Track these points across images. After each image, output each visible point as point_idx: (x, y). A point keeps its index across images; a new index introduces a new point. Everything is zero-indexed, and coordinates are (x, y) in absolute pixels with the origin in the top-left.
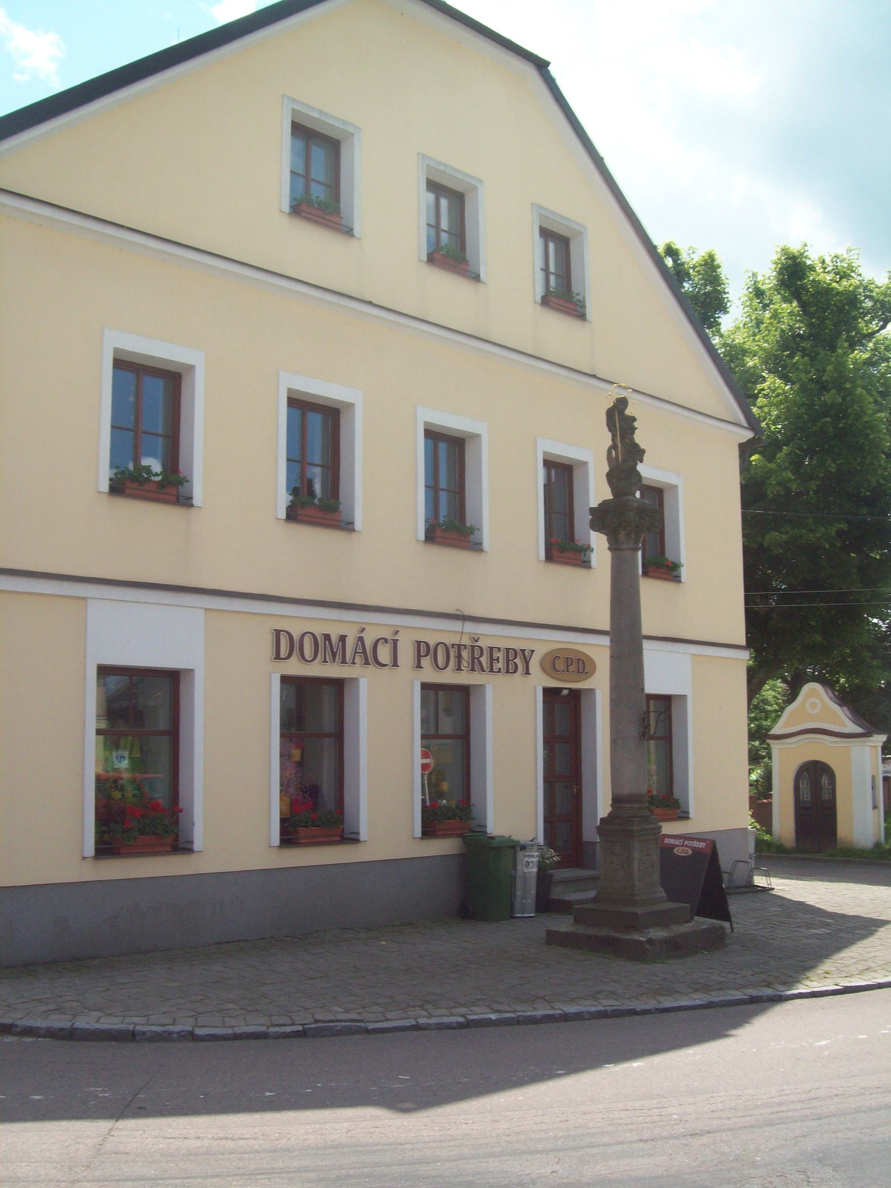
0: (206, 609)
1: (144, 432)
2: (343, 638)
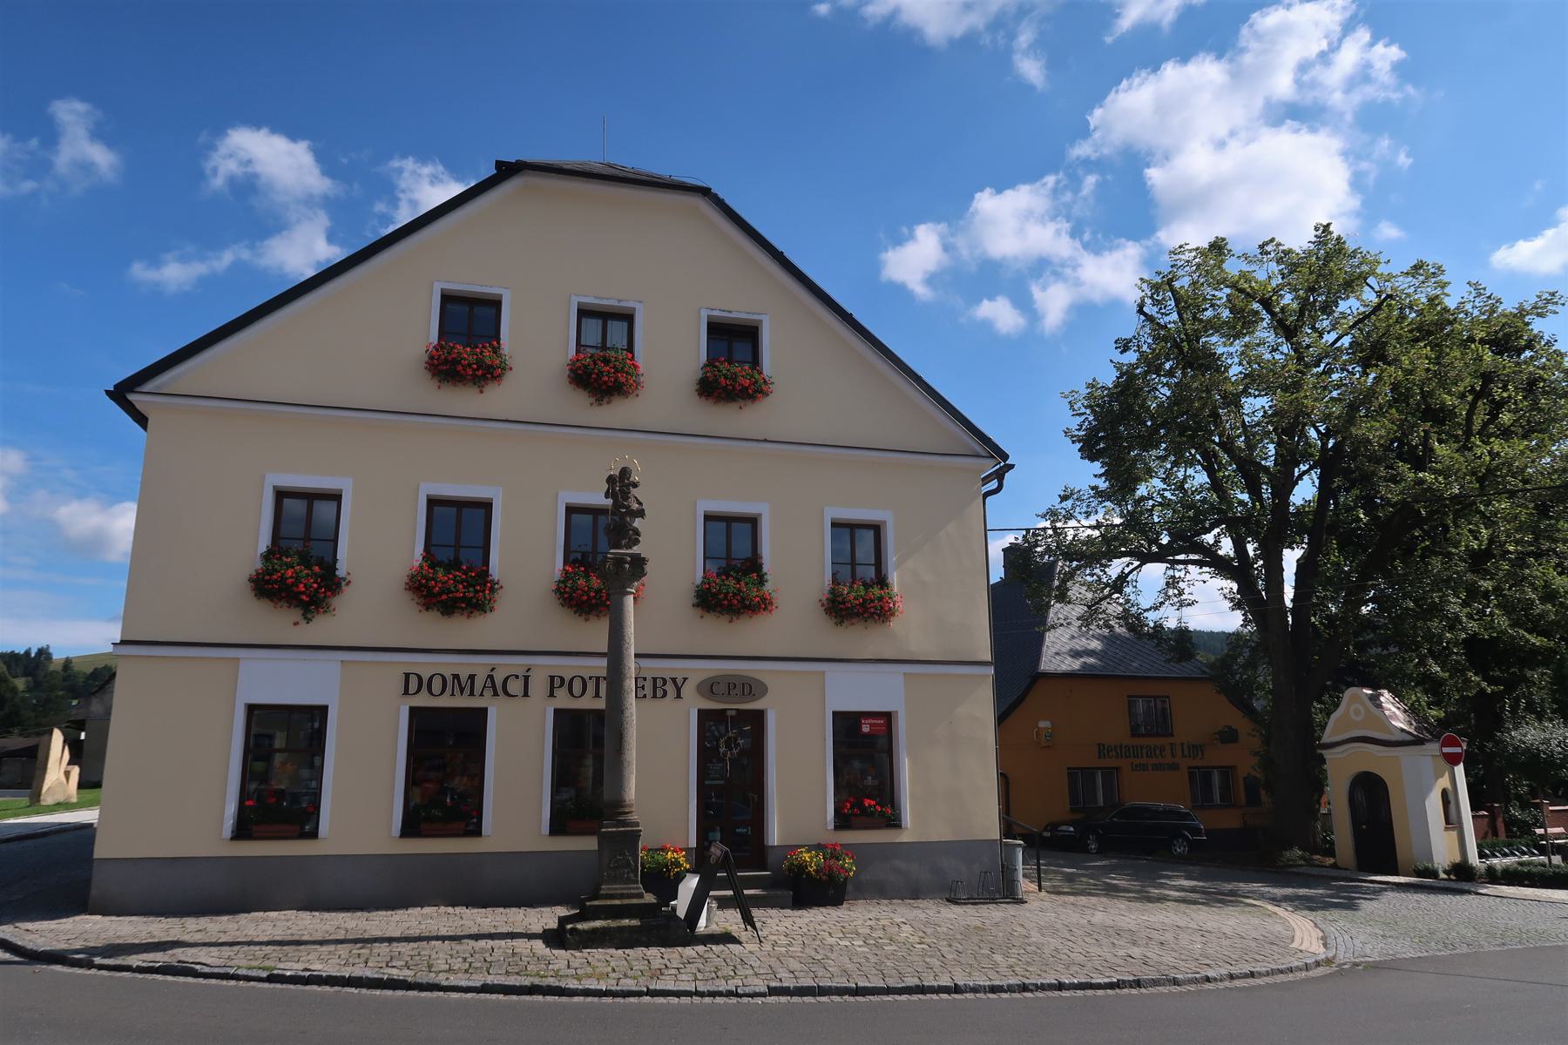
2: (472, 677)
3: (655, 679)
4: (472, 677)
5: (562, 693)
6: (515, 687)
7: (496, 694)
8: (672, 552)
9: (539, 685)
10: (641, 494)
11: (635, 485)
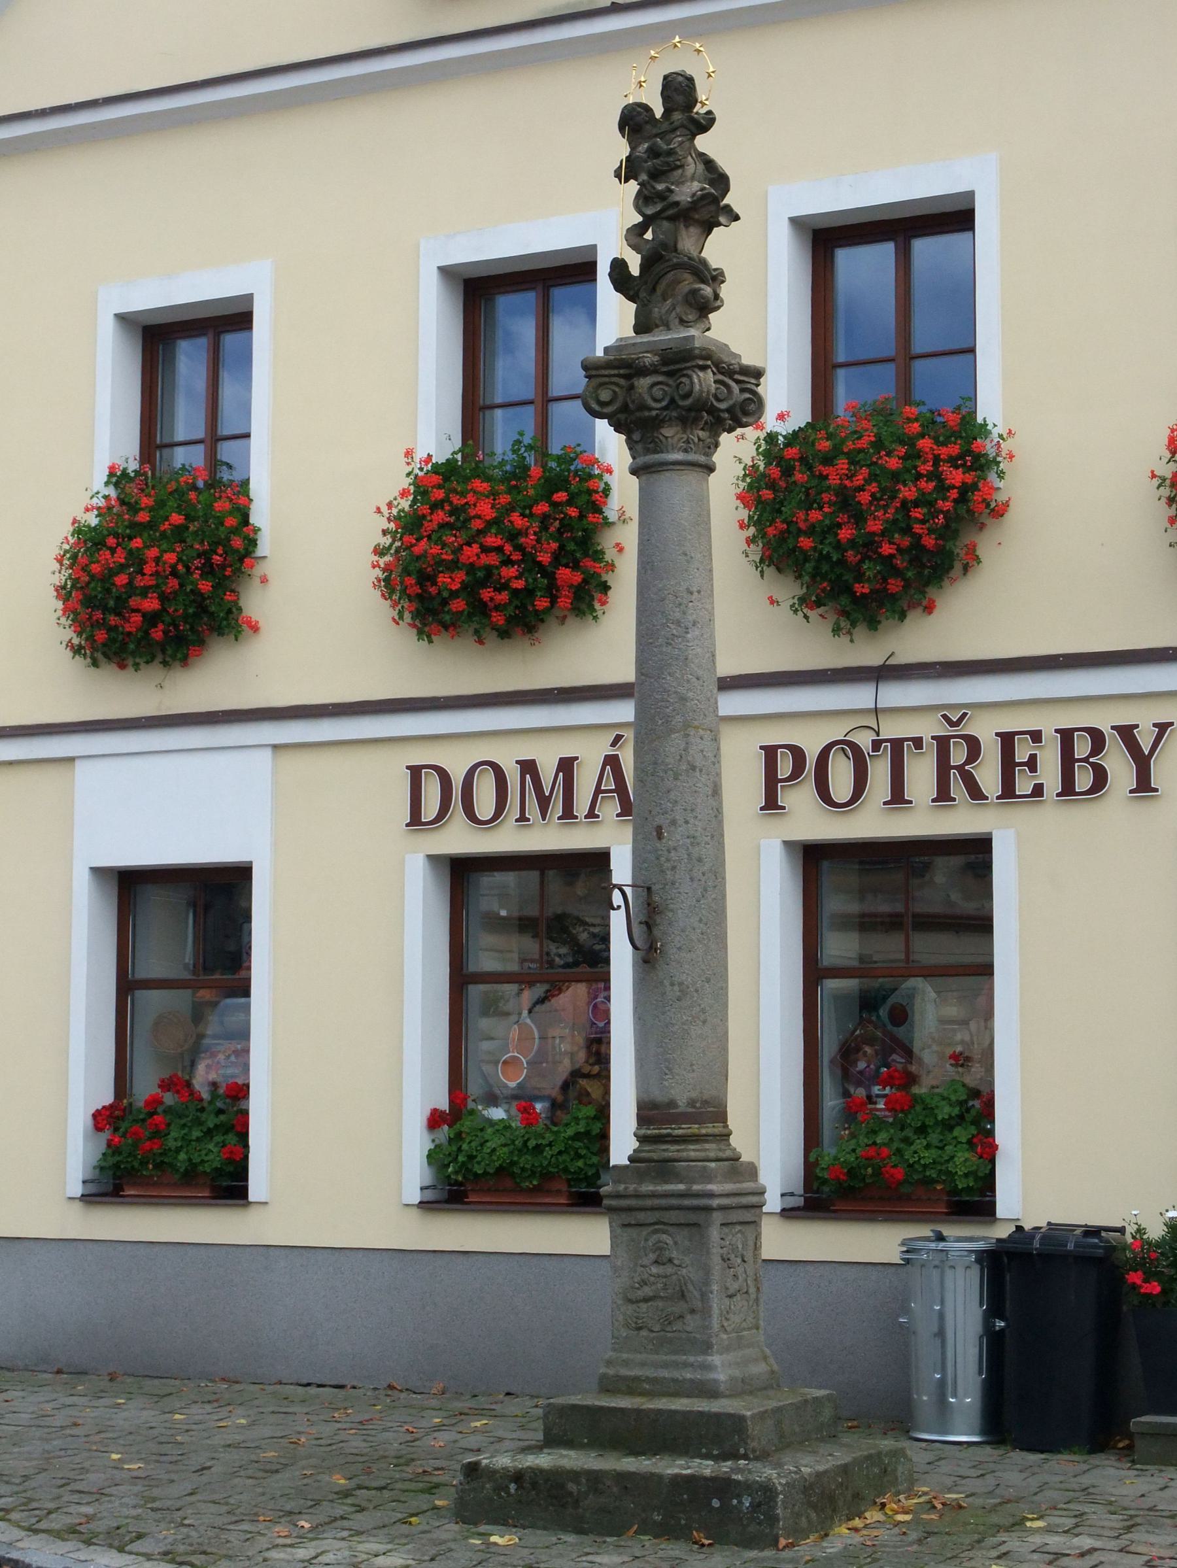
0: (275, 747)
1: (531, 402)
2: (566, 766)
3: (1066, 736)
4: (566, 766)
5: (800, 798)
10: (707, 98)
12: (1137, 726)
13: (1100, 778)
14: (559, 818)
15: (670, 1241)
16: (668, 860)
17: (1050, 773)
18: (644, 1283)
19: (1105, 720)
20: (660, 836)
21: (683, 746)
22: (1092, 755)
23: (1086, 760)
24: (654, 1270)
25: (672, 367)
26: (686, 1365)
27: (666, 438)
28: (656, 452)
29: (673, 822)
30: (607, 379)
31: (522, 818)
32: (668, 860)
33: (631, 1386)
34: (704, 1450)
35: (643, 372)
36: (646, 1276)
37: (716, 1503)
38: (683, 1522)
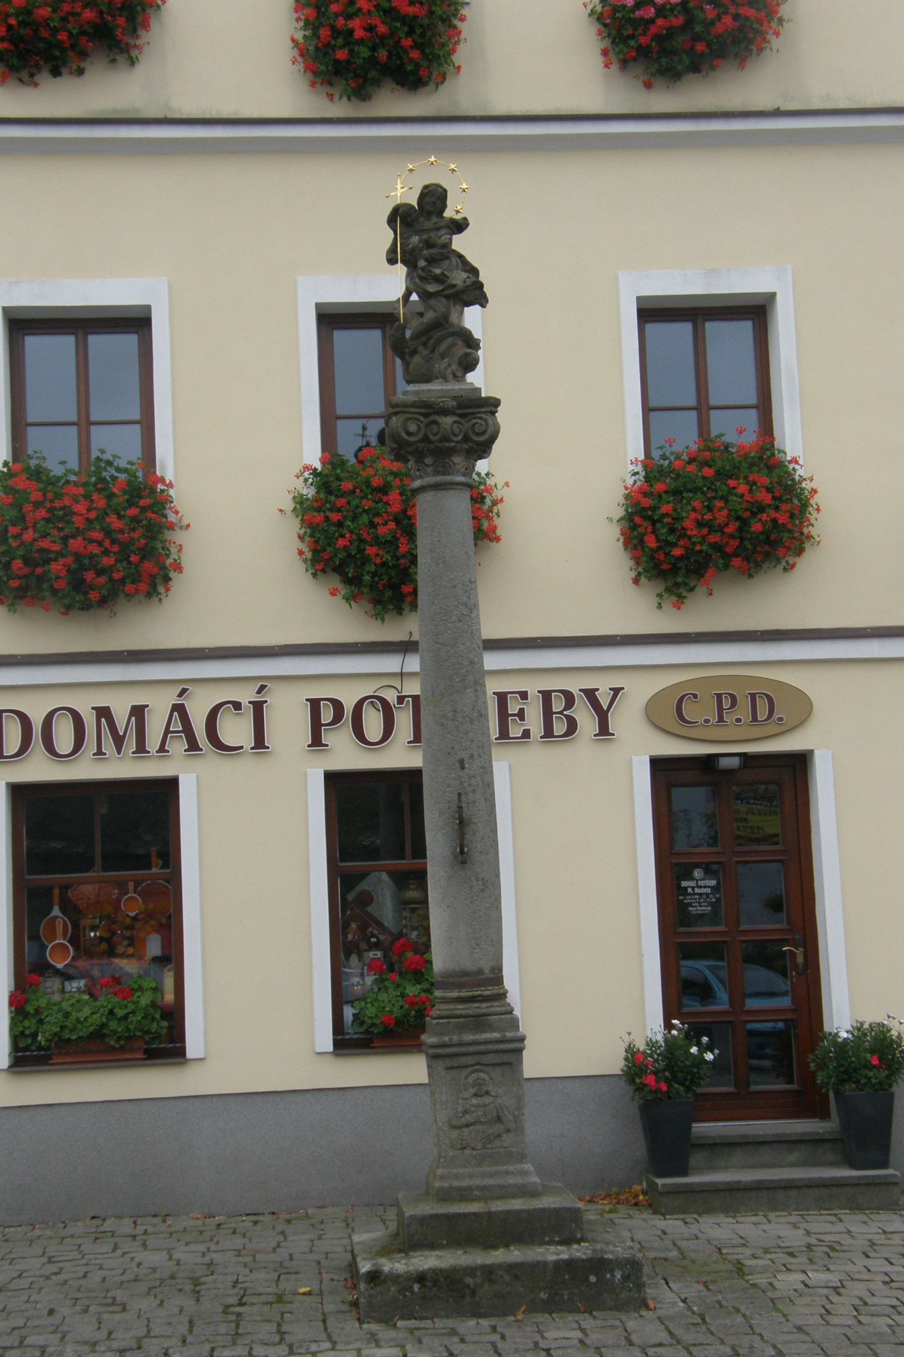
2: (138, 712)
3: (546, 696)
4: (138, 712)
6: (236, 730)
7: (193, 745)
8: (567, 440)
9: (288, 719)
11: (460, 226)
12: (598, 690)
13: (572, 726)
14: (133, 753)
15: (486, 1077)
16: (470, 785)
17: (534, 721)
18: (466, 1112)
19: (574, 685)
20: (462, 767)
21: (474, 698)
22: (566, 709)
23: (561, 713)
24: (474, 1101)
25: (466, 411)
26: (507, 1173)
27: (455, 464)
28: (444, 474)
29: (472, 756)
30: (412, 416)
31: (99, 752)
32: (470, 785)
33: (464, 1195)
34: (547, 1239)
35: (445, 412)
36: (468, 1106)
37: (593, 1279)
38: (566, 1297)
